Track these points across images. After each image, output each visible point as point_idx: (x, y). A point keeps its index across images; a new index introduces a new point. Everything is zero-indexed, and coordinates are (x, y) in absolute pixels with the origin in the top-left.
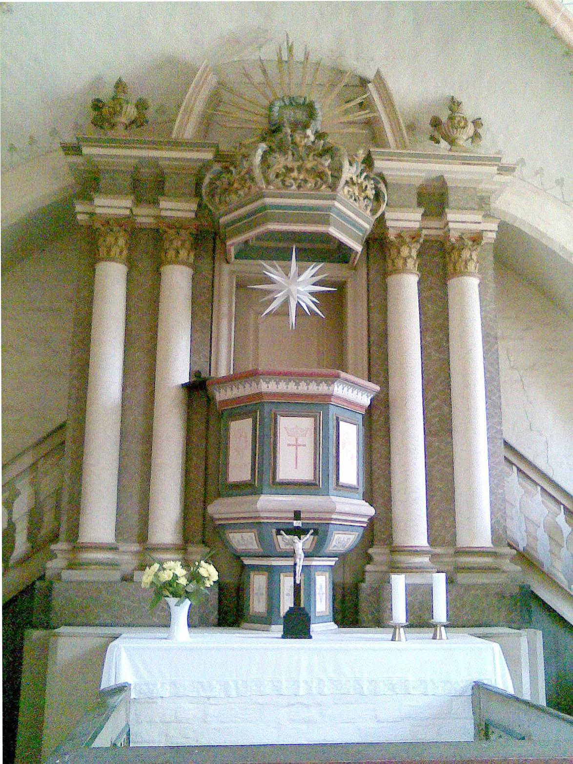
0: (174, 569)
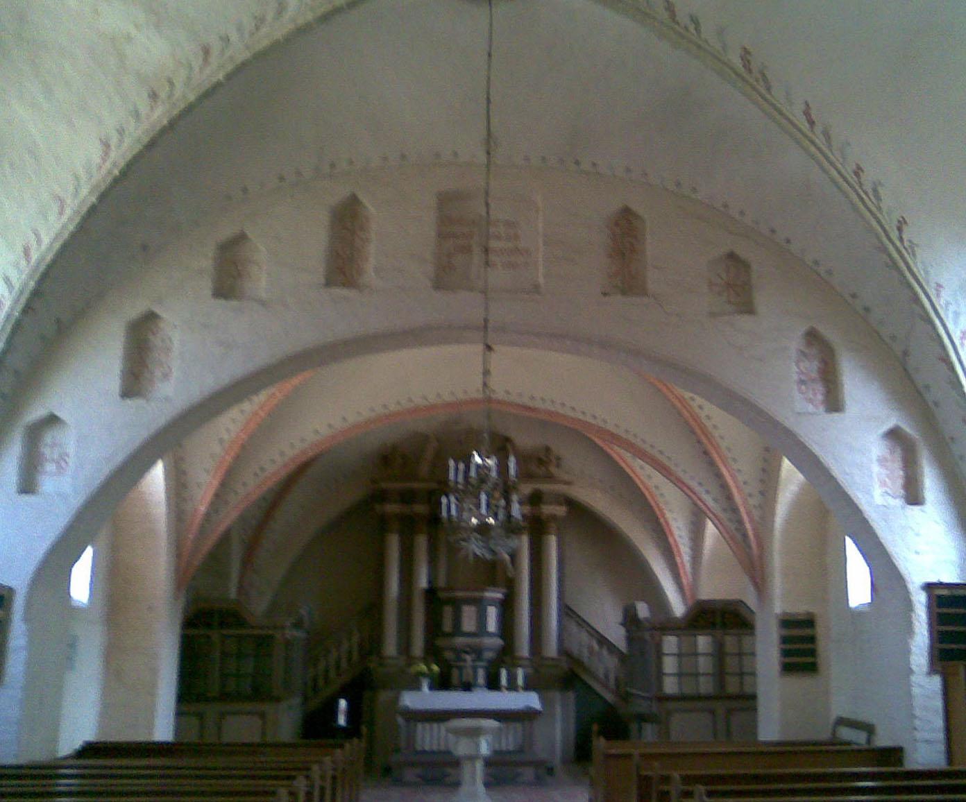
0: (423, 668)
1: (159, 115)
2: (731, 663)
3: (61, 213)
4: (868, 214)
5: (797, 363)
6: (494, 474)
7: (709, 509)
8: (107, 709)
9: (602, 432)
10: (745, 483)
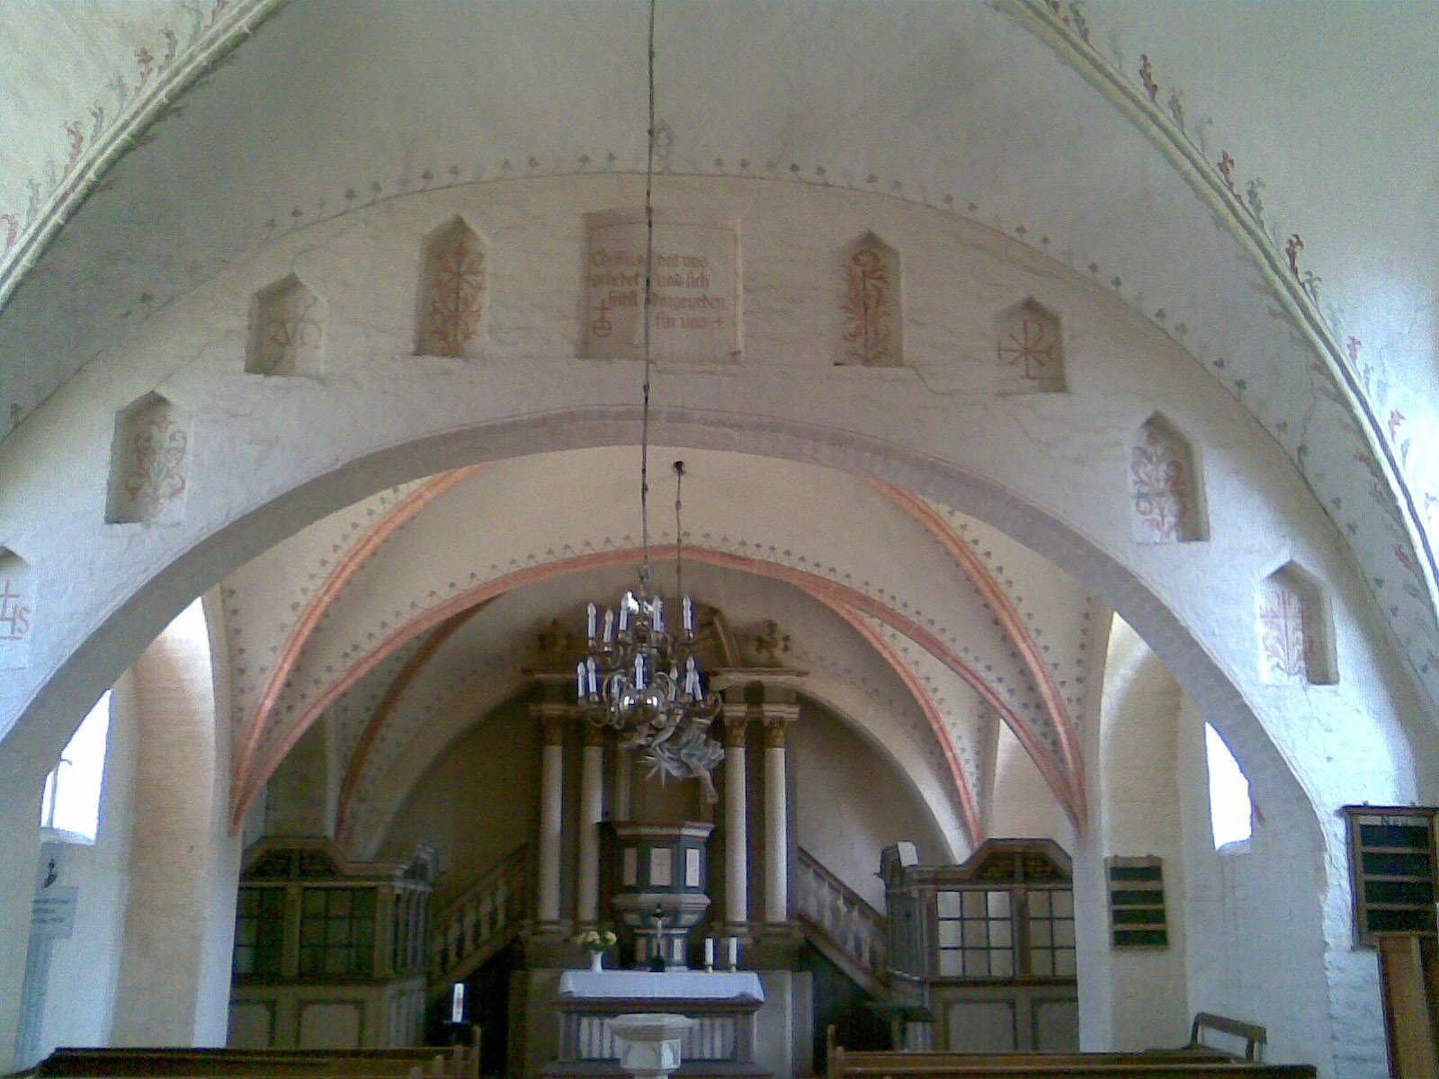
0: (594, 936)
1: (153, 88)
2: (1038, 932)
4: (1242, 232)
5: (1135, 466)
6: (658, 625)
7: (1001, 703)
8: (126, 998)
9: (843, 592)
10: (1056, 666)
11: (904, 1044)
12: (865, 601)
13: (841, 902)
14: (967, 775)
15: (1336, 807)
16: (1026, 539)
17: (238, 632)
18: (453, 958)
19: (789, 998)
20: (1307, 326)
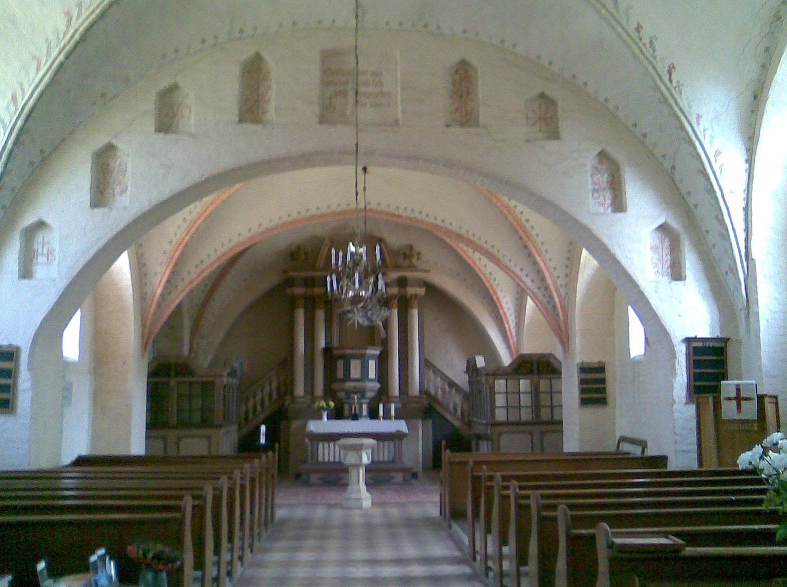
2: (544, 399)
3: (38, 69)
6: (365, 258)
8: (96, 434)
9: (449, 232)
10: (555, 268)
11: (477, 450)
12: (460, 237)
13: (446, 386)
14: (510, 322)
15: (683, 338)
16: (539, 210)
17: (143, 255)
18: (251, 416)
19: (420, 433)
20: (676, 109)
